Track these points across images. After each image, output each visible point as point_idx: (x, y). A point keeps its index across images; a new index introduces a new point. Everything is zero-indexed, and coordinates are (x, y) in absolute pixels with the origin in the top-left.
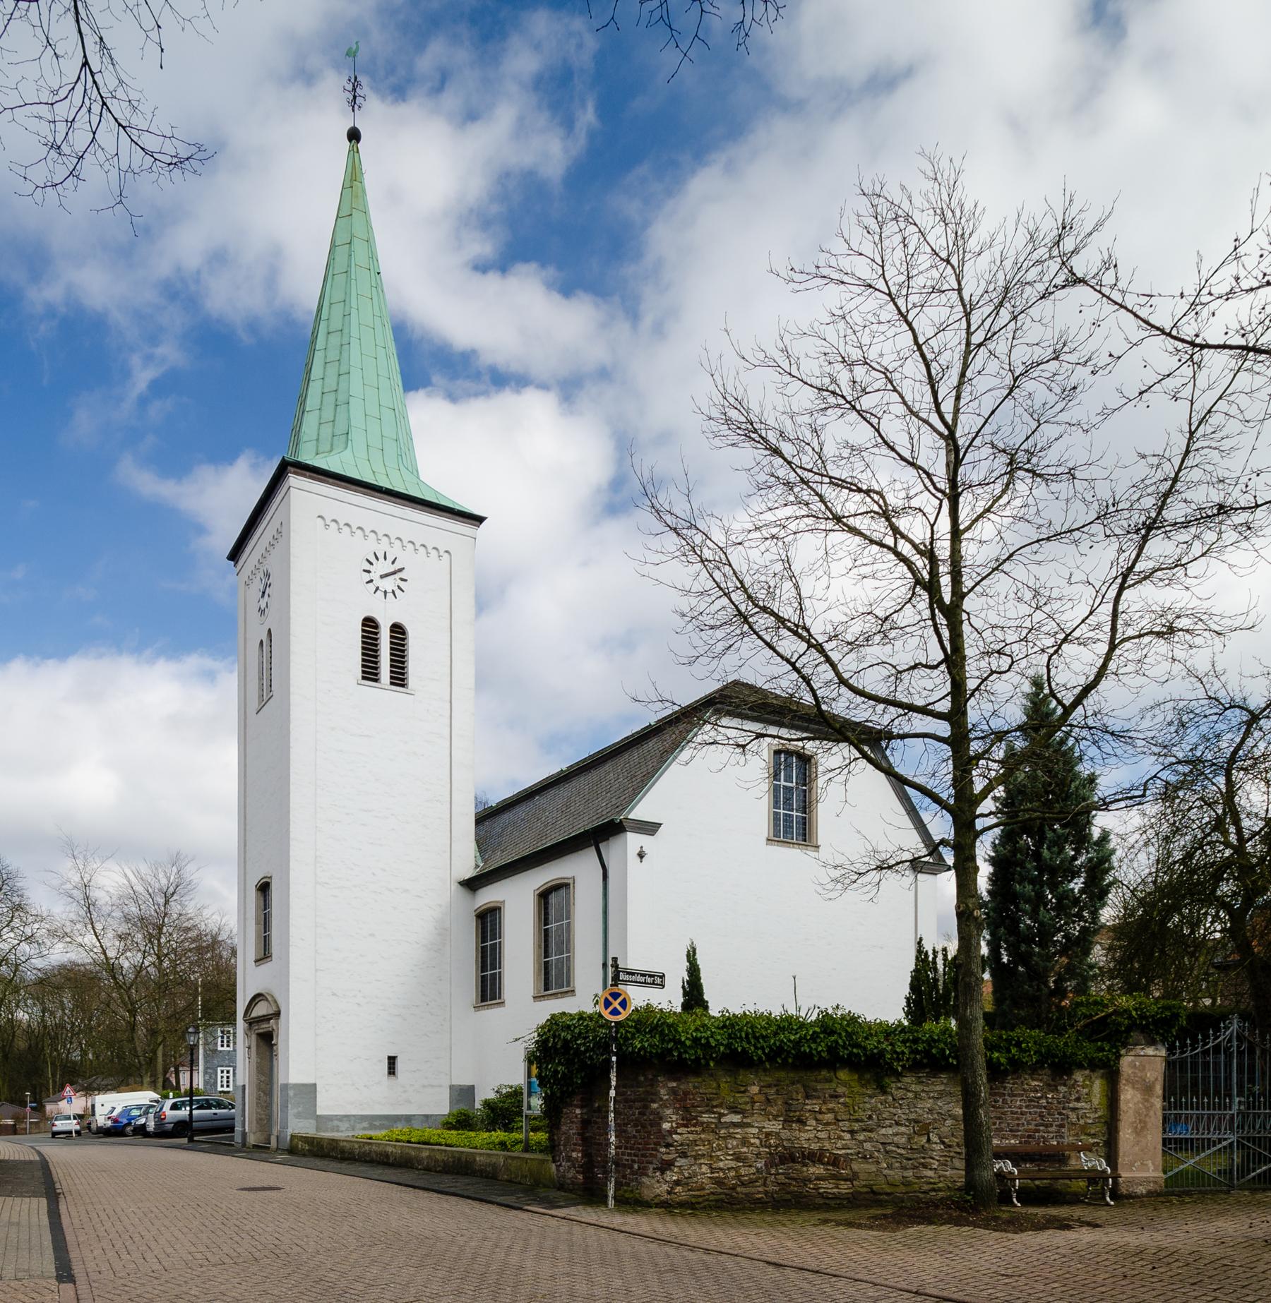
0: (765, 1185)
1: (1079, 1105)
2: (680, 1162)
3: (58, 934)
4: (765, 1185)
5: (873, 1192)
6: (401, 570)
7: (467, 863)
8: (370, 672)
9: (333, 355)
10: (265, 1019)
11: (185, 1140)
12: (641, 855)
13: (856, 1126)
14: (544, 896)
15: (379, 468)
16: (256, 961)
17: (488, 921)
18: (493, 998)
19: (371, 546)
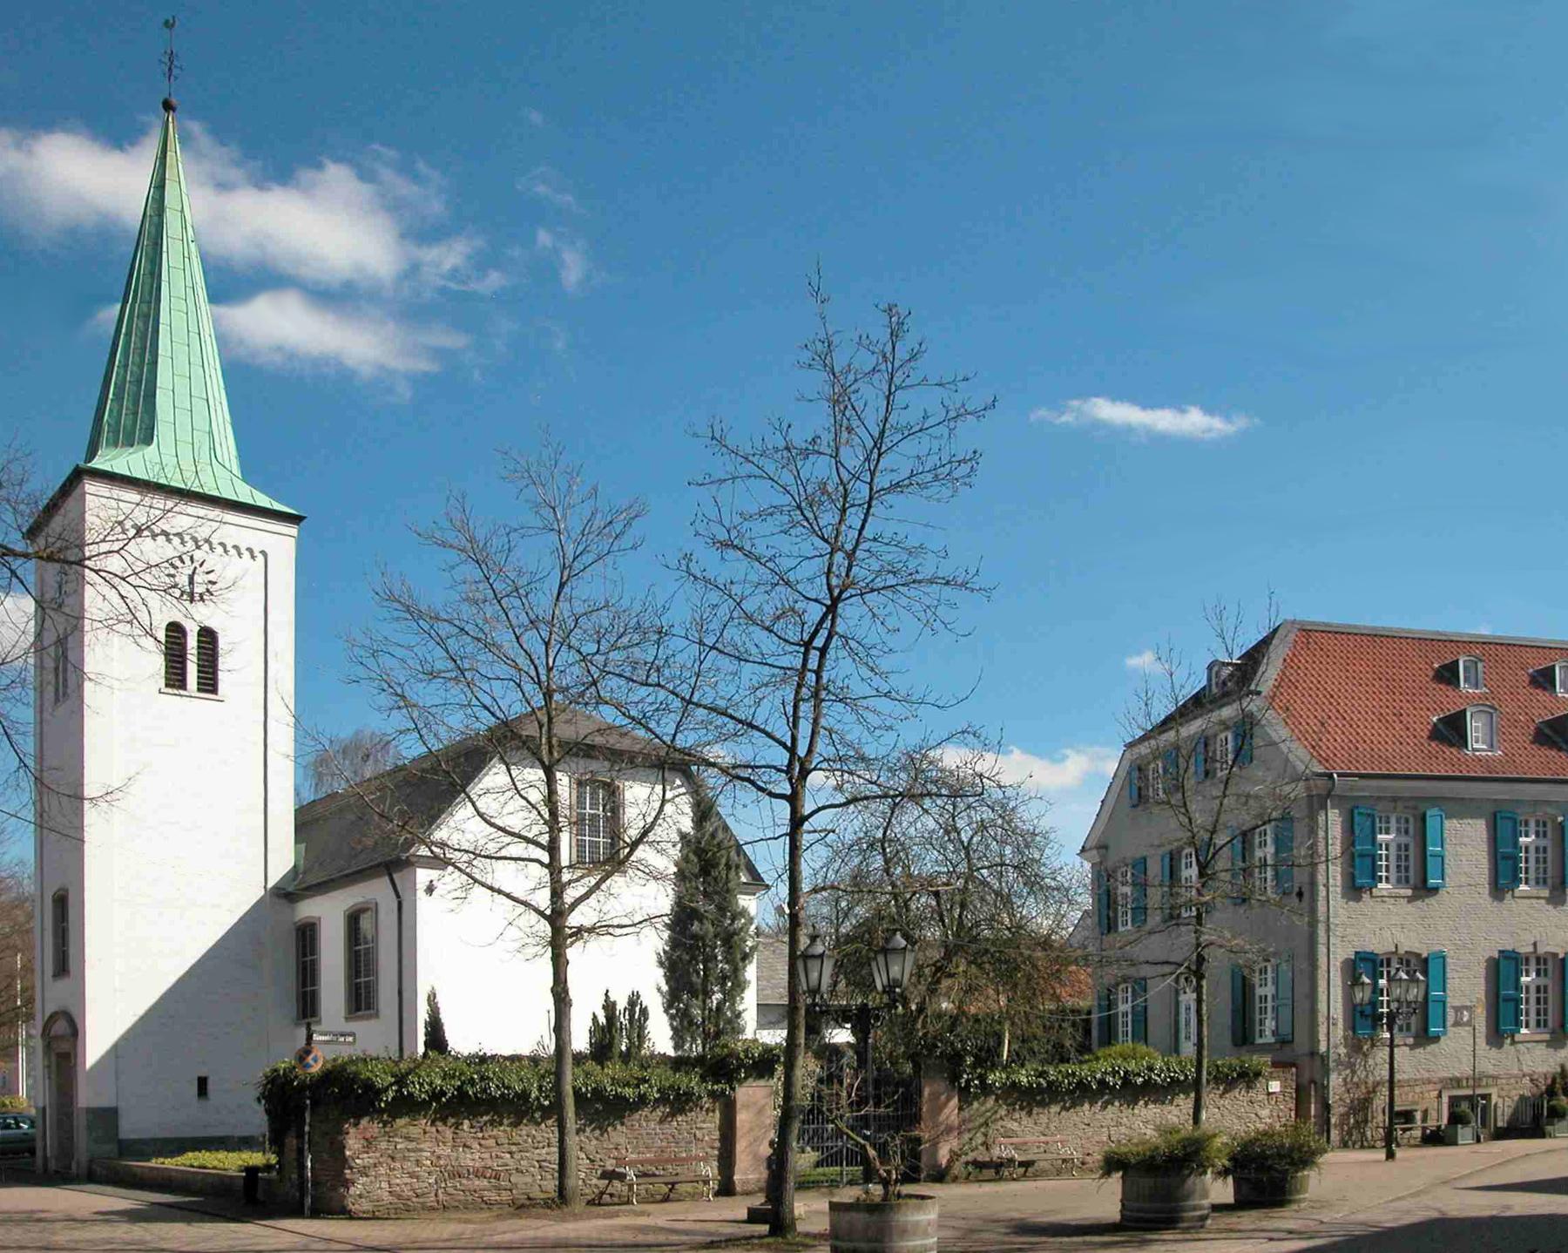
8: (175, 678)
12: (430, 889)
13: (514, 1148)
17: (307, 935)
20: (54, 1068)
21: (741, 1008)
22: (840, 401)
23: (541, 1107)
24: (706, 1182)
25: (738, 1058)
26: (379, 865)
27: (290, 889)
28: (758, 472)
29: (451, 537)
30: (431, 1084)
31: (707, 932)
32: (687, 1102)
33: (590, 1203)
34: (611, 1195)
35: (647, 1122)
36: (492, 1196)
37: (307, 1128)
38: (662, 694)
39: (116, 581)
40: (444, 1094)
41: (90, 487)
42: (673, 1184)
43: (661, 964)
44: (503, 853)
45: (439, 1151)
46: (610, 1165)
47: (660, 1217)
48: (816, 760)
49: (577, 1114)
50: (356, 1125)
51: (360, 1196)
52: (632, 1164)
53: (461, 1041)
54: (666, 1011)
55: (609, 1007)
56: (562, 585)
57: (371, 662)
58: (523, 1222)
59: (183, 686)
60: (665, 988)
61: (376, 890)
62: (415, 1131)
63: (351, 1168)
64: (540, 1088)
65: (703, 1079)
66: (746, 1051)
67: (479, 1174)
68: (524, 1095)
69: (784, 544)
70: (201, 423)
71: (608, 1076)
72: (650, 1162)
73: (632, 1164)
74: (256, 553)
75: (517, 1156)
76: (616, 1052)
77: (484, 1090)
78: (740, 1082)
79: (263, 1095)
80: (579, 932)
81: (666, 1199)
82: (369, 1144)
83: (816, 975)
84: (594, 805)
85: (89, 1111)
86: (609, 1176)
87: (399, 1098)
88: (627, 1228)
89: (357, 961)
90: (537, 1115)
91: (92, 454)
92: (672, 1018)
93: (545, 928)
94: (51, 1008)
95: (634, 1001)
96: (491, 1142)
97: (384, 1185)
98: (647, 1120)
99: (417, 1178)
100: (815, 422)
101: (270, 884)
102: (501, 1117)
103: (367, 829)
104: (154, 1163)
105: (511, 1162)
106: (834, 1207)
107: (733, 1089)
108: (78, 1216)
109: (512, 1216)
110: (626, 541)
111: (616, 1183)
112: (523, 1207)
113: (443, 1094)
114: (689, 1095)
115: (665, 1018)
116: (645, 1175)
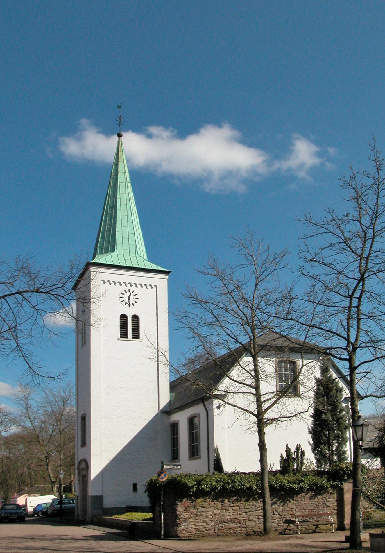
0: (214, 530)
1: (330, 500)
2: (184, 524)
3: (13, 421)
4: (214, 530)
5: (254, 531)
6: (129, 305)
8: (124, 334)
11: (58, 518)
12: (219, 407)
13: (247, 510)
15: (127, 257)
17: (174, 427)
20: (81, 480)
21: (345, 449)
22: (358, 198)
23: (258, 493)
24: (331, 525)
25: (343, 471)
26: (199, 399)
27: (169, 410)
28: (325, 231)
29: (210, 271)
30: (211, 484)
31: (328, 418)
32: (322, 490)
33: (281, 533)
34: (290, 530)
35: (304, 499)
36: (238, 530)
37: (162, 503)
38: (292, 322)
39: (60, 298)
40: (217, 488)
41: (93, 269)
42: (317, 525)
43: (310, 432)
44: (240, 391)
45: (215, 512)
46: (289, 517)
47: (308, 540)
48: (359, 342)
49: (271, 496)
50: (181, 501)
51: (183, 530)
52: (298, 517)
53: (228, 467)
54: (313, 452)
55: (288, 451)
56: (256, 285)
57: (184, 320)
58: (247, 542)
59: (127, 337)
60: (312, 442)
61: (198, 409)
62: (205, 504)
63: (179, 519)
64: (257, 485)
65: (328, 480)
66: (347, 467)
67: (232, 521)
68: (251, 488)
69: (341, 257)
70: (132, 242)
71: (285, 480)
72: (306, 516)
73: (298, 517)
74: (148, 286)
75: (248, 514)
76: (291, 469)
77: (233, 487)
78: (345, 480)
79: (147, 490)
80: (272, 420)
81: (314, 532)
82: (186, 509)
83: (360, 433)
84: (286, 370)
85: (93, 497)
86: (289, 522)
87: (198, 490)
88: (290, 545)
89: (193, 437)
90: (256, 496)
91: (94, 257)
92: (316, 454)
93: (254, 419)
94: (80, 458)
95: (298, 448)
96: (237, 508)
97: (193, 526)
98: (304, 498)
99: (207, 523)
100: (351, 208)
101: (161, 408)
102: (241, 498)
103: (195, 387)
104: (114, 517)
105: (246, 516)
106: (371, 535)
107: (342, 484)
108: (77, 537)
109: (245, 539)
110: (282, 265)
111: (291, 525)
112: (248, 536)
113: (217, 488)
114: (322, 486)
115: (313, 455)
116: (304, 521)
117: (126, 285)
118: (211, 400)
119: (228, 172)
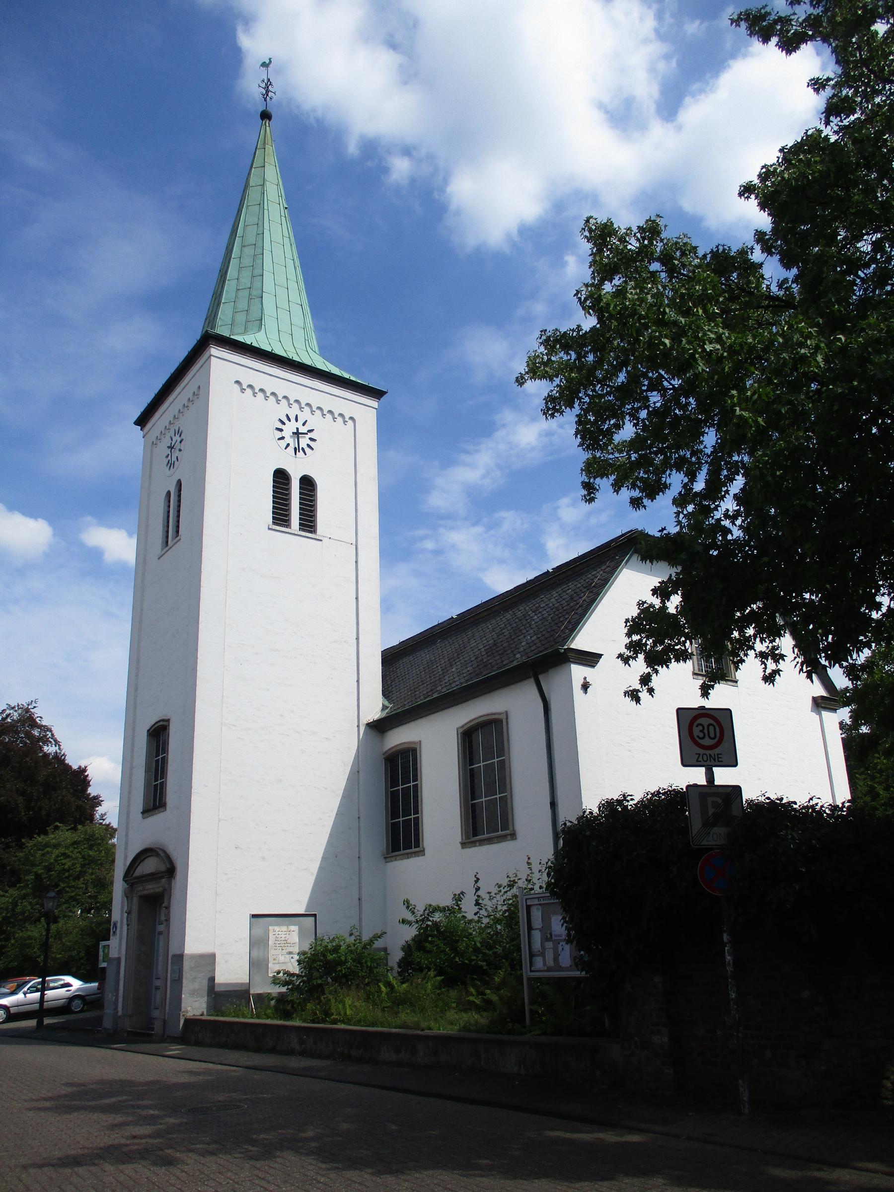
7: (374, 707)
8: (281, 517)
9: (247, 261)
10: (153, 877)
12: (585, 687)
14: (468, 737)
16: (143, 813)
18: (408, 846)
19: (283, 410)
20: (135, 908)
59: (288, 526)
117: (290, 405)
118: (567, 664)
119: (624, 130)
